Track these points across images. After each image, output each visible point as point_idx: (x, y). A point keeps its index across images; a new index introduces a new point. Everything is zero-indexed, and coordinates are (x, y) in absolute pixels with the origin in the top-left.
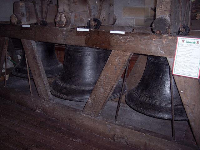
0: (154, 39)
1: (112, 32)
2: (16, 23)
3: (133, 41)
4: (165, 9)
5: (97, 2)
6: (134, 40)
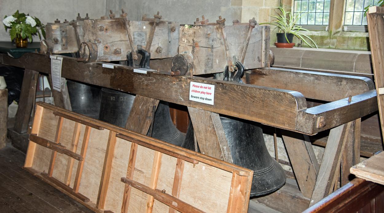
0: (174, 82)
1: (136, 71)
2: (45, 53)
3: (155, 83)
4: (188, 44)
5: (144, 27)
6: (156, 82)
